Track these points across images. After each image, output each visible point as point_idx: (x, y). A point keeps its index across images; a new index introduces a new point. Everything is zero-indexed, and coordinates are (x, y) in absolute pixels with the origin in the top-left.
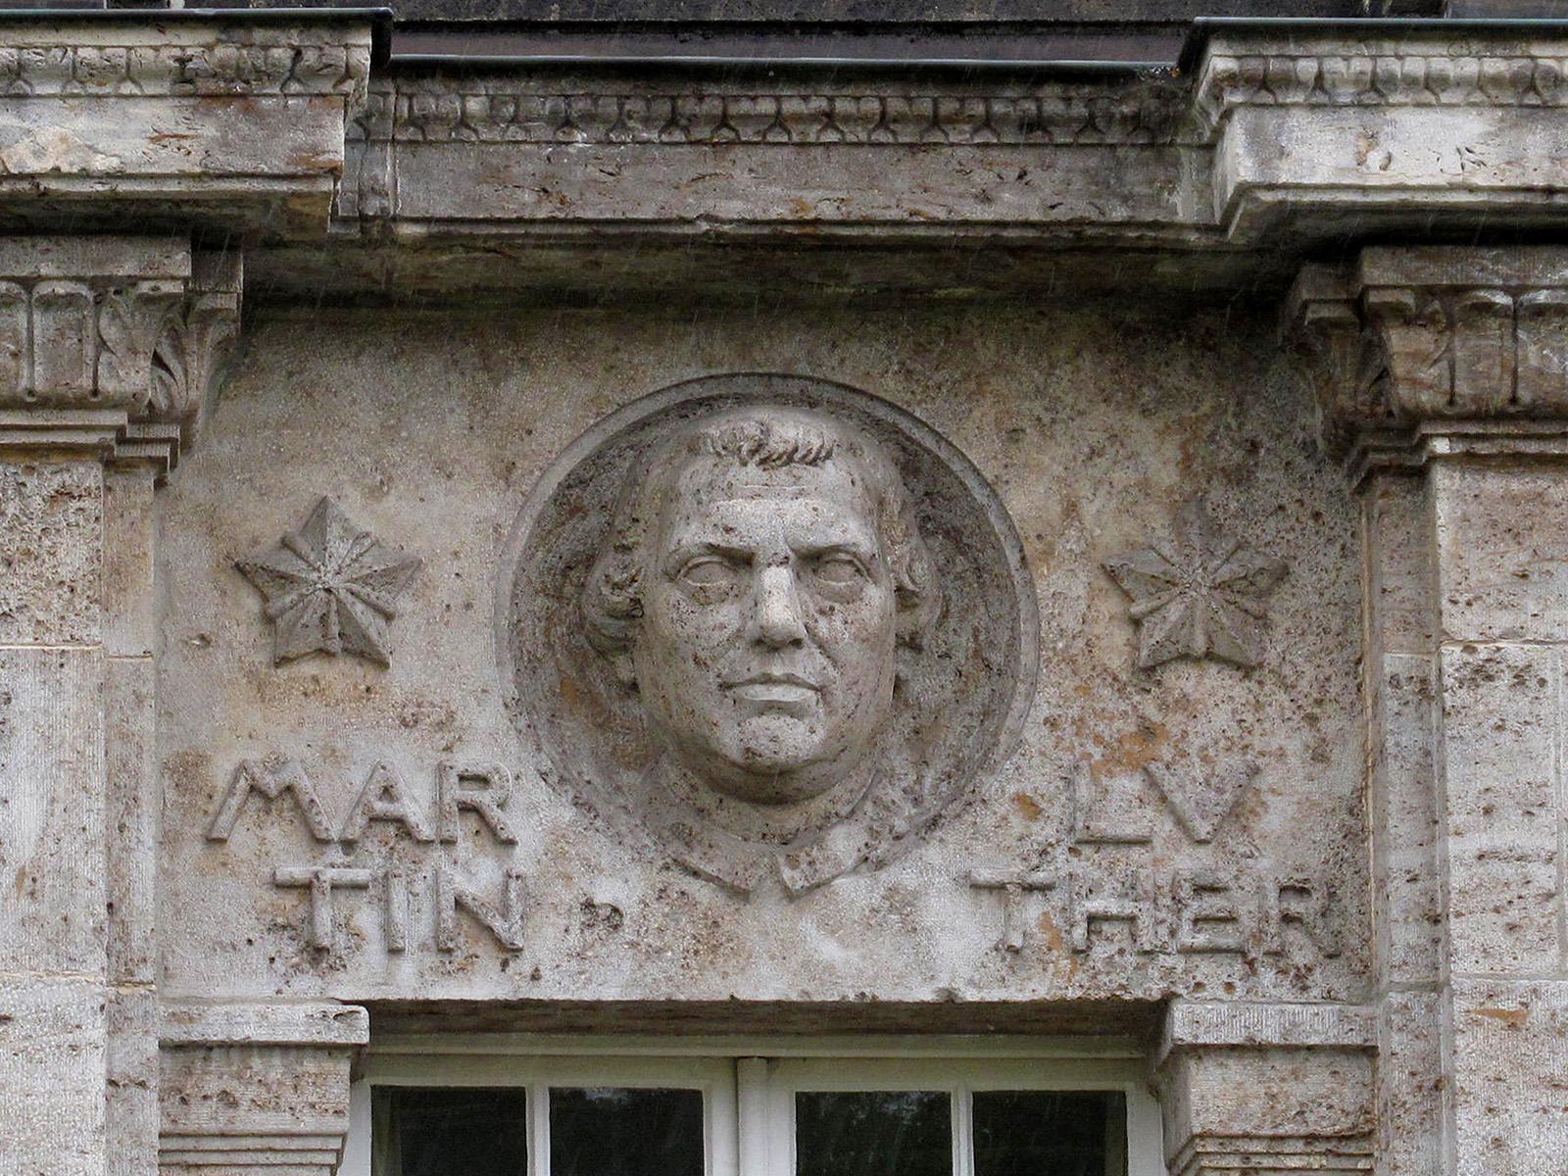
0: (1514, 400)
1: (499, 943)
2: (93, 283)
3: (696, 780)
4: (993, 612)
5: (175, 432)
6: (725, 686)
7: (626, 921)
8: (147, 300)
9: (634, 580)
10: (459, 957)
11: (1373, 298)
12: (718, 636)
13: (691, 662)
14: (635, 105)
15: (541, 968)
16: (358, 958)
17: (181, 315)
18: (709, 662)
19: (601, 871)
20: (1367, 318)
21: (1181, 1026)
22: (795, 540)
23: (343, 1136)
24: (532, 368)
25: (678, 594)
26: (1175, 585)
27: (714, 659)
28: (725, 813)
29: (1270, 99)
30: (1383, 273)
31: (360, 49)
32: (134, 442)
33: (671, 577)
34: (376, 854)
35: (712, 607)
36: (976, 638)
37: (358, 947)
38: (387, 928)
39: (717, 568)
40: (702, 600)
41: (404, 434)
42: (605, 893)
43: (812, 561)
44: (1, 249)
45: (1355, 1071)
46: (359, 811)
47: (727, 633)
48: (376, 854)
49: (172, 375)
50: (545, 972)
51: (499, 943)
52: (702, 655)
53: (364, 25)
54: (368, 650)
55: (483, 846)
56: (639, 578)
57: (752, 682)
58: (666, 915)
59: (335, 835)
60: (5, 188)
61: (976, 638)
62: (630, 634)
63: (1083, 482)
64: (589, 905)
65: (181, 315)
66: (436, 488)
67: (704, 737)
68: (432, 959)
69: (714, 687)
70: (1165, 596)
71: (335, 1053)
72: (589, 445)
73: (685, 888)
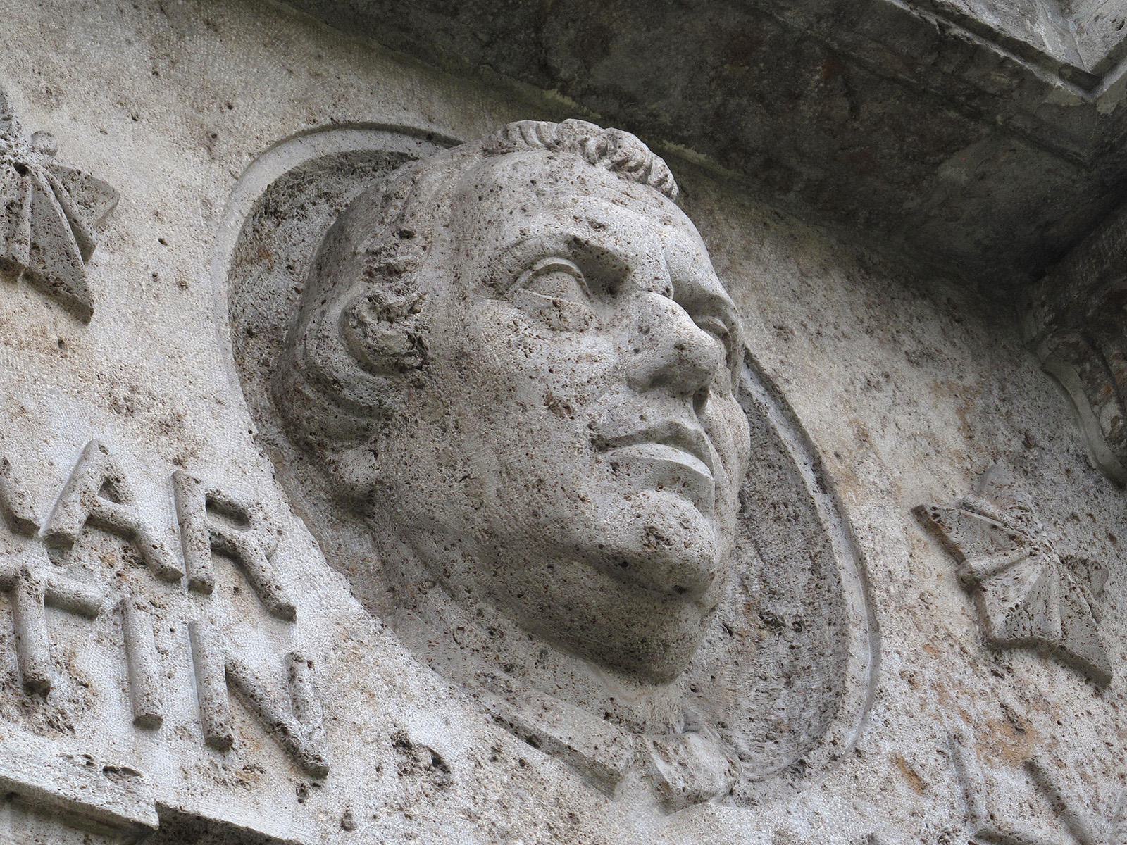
1: (292, 751)
3: (502, 621)
4: (770, 554)
6: (601, 445)
7: (456, 777)
9: (413, 311)
10: (236, 759)
12: (585, 370)
13: (542, 410)
15: (353, 811)
16: (88, 720)
18: (574, 405)
19: (411, 698)
22: (681, 269)
24: (6, 280)
25: (513, 313)
26: (1021, 543)
27: (582, 401)
28: (549, 673)
33: (497, 288)
34: (97, 575)
35: (568, 335)
36: (746, 589)
37: (88, 705)
38: (132, 684)
39: (572, 283)
40: (555, 321)
41: (70, 45)
42: (424, 731)
46: (76, 496)
47: (599, 368)
48: (97, 575)
50: (359, 818)
51: (292, 751)
52: (560, 394)
54: (68, 280)
55: (247, 612)
56: (422, 308)
57: (648, 436)
58: (507, 786)
59: (43, 522)
61: (746, 589)
62: (388, 402)
64: (402, 744)
66: (120, 124)
67: (559, 520)
68: (199, 755)
69: (585, 442)
70: (1014, 555)
72: (297, 156)
73: (523, 755)
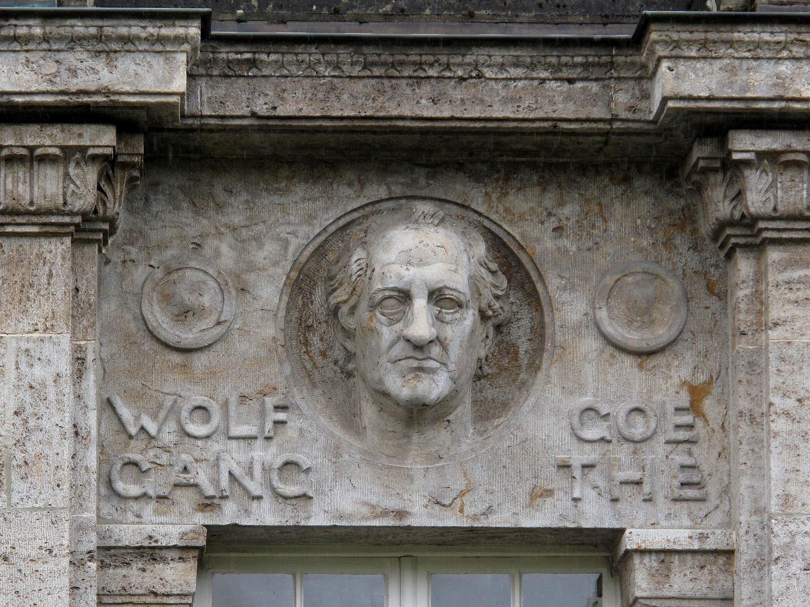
0: (775, 209)
2: (62, 148)
5: (106, 227)
8: (94, 158)
11: (736, 156)
14: (289, 57)
17: (109, 165)
20: (732, 169)
21: (630, 541)
23: (193, 595)
29: (132, 48)
30: (745, 144)
31: (194, 30)
32: (84, 230)
43: (437, 296)
44: (1, 130)
45: (716, 566)
49: (106, 195)
53: (198, 18)
60: (4, 99)
63: (598, 257)
65: (109, 165)
71: (108, 484)
